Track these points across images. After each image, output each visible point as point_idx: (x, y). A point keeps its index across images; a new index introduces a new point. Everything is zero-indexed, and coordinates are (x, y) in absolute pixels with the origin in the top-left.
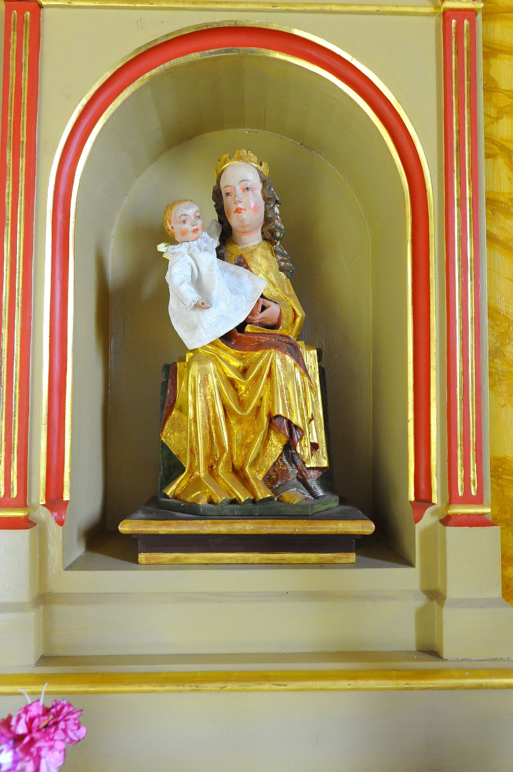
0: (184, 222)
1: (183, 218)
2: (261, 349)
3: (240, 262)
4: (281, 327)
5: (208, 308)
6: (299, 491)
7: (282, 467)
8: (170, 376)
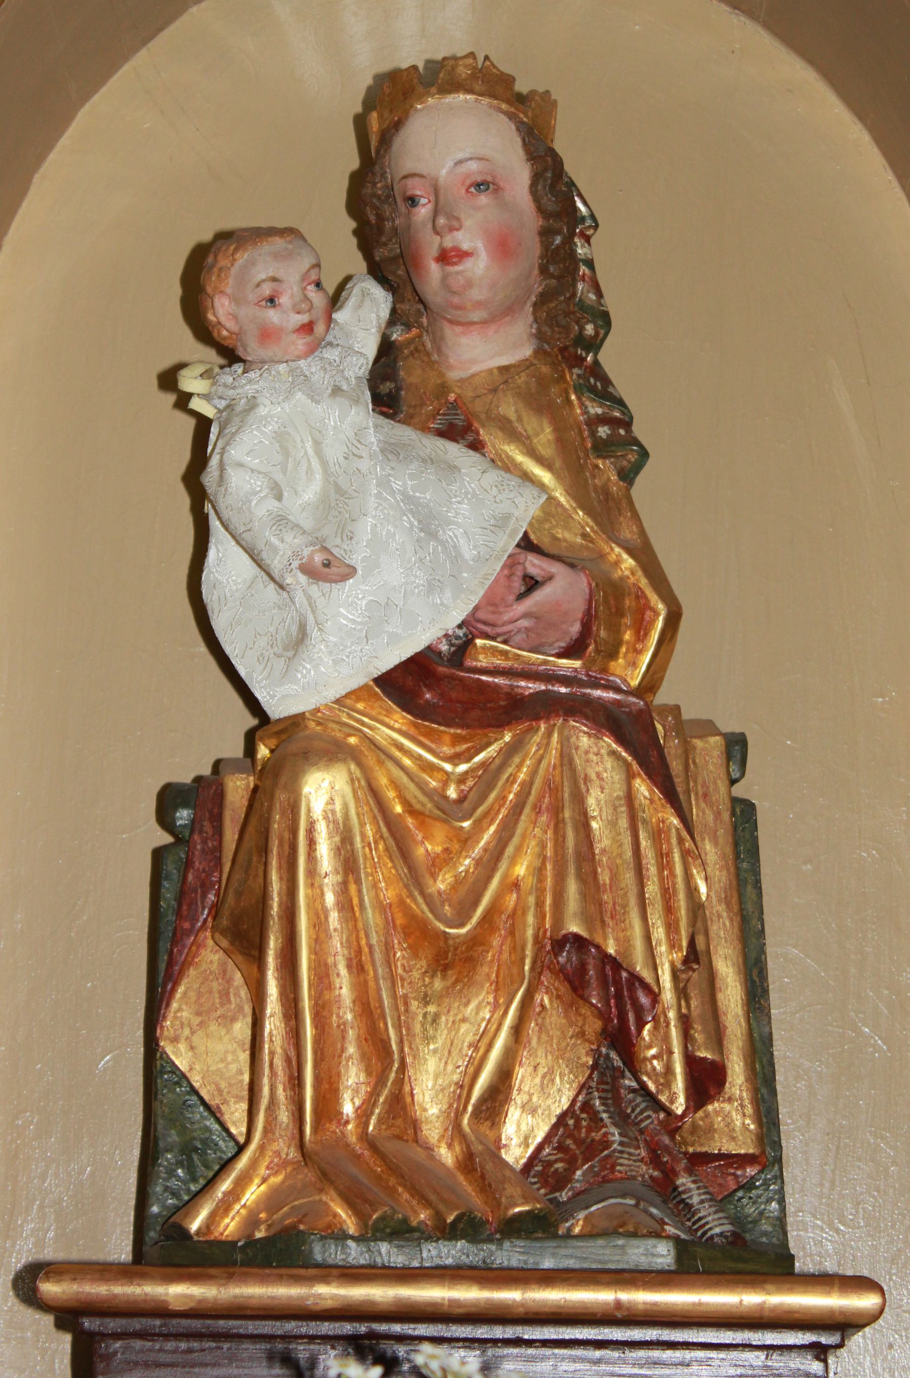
0: (271, 300)
1: (267, 290)
2: (518, 719)
3: (452, 426)
4: (591, 647)
5: (344, 578)
6: (646, 1211)
7: (589, 1130)
8: (396, 946)
